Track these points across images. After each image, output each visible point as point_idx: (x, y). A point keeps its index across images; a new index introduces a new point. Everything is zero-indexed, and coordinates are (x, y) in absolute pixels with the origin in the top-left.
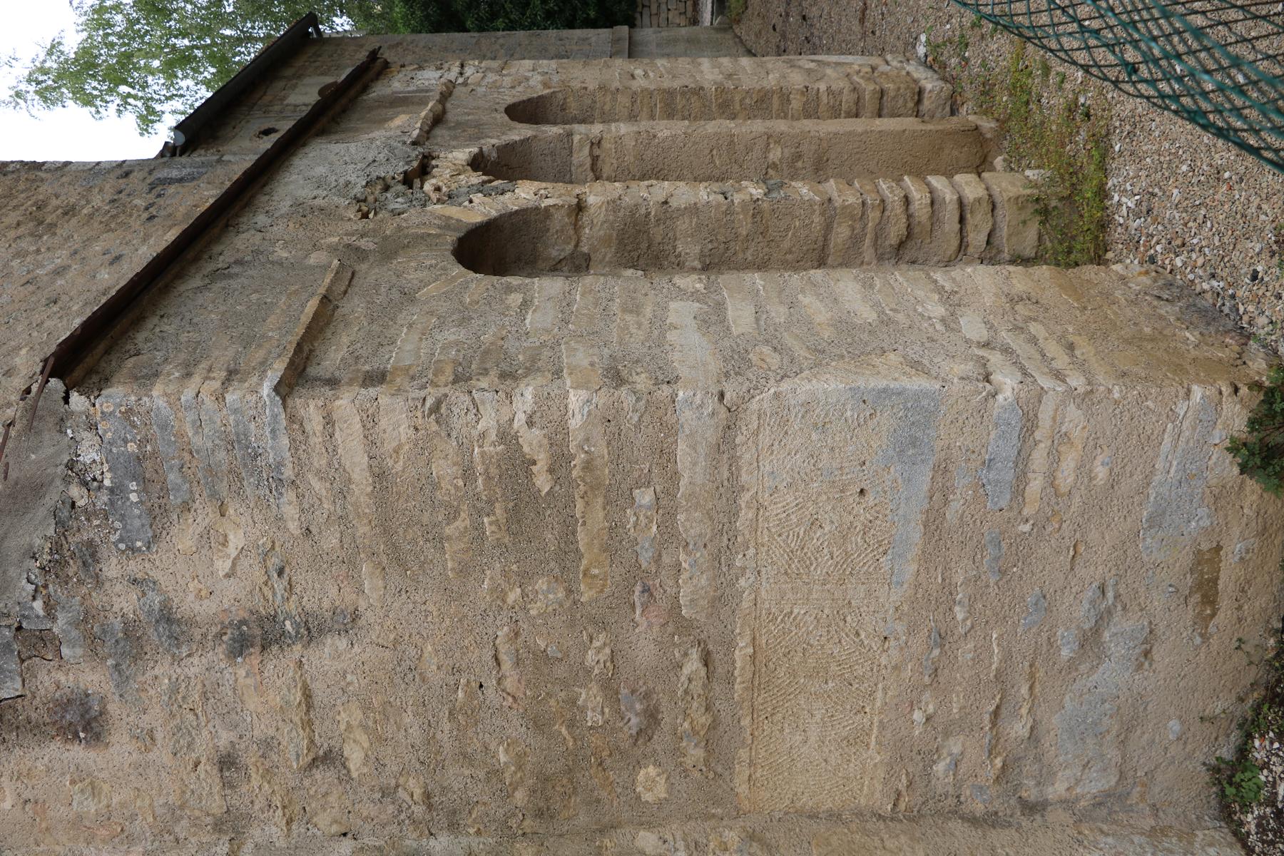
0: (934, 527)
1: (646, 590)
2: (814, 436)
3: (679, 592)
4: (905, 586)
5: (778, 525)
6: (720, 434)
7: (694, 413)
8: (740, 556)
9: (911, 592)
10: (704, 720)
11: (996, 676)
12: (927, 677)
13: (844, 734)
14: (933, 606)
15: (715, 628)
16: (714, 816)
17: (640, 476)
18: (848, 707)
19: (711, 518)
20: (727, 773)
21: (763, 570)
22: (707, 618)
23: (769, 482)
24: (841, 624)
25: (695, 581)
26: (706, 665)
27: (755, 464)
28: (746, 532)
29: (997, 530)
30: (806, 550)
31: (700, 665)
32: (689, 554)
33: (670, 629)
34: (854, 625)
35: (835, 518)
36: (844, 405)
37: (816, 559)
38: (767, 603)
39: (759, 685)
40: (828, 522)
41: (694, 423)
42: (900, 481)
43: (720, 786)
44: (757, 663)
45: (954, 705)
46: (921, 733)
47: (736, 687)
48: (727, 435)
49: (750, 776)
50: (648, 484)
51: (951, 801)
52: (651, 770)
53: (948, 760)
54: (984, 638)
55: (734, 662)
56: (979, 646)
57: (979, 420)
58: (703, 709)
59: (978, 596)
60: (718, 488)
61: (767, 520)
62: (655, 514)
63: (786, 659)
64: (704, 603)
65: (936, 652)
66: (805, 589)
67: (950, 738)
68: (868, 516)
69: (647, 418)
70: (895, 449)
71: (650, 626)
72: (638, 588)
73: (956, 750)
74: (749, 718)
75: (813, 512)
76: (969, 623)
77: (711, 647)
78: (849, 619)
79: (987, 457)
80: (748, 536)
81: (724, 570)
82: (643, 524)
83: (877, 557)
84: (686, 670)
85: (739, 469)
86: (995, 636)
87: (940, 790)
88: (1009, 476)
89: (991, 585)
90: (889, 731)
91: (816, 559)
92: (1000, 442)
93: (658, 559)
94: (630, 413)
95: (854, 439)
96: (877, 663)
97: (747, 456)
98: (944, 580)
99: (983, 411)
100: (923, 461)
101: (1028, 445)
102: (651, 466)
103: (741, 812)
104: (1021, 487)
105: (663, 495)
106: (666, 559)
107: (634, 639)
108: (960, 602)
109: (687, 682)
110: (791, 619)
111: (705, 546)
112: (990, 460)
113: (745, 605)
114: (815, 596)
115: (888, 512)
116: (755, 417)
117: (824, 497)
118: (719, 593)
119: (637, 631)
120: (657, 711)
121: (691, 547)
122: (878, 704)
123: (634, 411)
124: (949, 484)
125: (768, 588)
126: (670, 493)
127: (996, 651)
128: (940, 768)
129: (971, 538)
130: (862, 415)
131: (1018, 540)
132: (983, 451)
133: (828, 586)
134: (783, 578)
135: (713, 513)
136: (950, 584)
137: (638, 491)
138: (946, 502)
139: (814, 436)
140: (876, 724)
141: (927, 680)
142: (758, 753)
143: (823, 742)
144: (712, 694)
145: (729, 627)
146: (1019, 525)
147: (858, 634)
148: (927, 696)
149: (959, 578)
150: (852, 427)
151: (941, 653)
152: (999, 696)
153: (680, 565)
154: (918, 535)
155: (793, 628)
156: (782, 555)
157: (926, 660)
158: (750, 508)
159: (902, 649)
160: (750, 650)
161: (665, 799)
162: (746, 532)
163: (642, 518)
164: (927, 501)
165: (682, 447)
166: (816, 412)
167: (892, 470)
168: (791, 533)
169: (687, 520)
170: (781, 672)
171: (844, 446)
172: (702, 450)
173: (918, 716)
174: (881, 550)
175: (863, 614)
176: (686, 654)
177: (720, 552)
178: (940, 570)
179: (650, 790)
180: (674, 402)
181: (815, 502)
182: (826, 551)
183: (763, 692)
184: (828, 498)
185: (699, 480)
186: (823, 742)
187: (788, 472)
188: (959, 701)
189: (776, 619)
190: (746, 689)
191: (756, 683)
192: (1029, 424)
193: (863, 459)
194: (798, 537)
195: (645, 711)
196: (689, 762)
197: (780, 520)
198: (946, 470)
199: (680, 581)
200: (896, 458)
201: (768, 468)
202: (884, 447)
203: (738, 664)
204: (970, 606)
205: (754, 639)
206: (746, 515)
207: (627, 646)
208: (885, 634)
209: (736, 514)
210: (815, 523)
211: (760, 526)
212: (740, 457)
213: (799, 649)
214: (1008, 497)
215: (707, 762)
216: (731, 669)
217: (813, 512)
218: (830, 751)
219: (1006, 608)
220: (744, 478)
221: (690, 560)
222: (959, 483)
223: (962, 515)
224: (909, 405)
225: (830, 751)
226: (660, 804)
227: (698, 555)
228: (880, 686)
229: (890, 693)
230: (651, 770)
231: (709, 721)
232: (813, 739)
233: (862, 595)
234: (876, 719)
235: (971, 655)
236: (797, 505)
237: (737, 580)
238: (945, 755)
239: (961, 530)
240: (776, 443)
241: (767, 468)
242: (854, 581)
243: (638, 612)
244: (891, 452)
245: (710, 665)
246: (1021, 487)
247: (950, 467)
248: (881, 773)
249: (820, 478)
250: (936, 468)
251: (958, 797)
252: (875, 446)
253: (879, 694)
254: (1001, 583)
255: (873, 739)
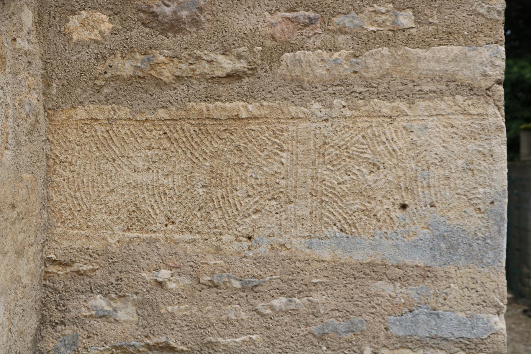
0: (368, 271)
1: (311, 21)
2: (460, 162)
3: (309, 50)
4: (308, 251)
5: (374, 135)
6: (466, 82)
7: (487, 59)
8: (344, 103)
9: (302, 256)
10: (167, 74)
11: (210, 342)
12: (209, 278)
13: (143, 207)
14: (285, 277)
15: (270, 83)
16: (49, 86)
17: (426, 15)
18: (175, 209)
19: (382, 77)
20: (102, 98)
21: (329, 124)
22: (280, 75)
23: (416, 125)
24: (269, 196)
25: (320, 64)
26: (228, 76)
27: (435, 113)
28: (367, 108)
29: (365, 328)
30: (348, 160)
31: (229, 70)
32: (347, 59)
33: (269, 43)
34: (267, 208)
35: (380, 184)
36: (490, 186)
37: (339, 170)
38: (294, 128)
39: (205, 125)
40: (375, 178)
41: (477, 59)
42: (415, 238)
43: (85, 91)
44: (229, 122)
45: (176, 307)
46: (143, 278)
47: (203, 103)
48: (464, 88)
49: (96, 120)
50: (418, 22)
51: (57, 316)
52: (107, 26)
53: (107, 308)
54: (251, 328)
55: (231, 101)
56: (243, 323)
57: (476, 302)
58: (178, 73)
59: (297, 317)
60: (413, 82)
61: (379, 125)
62: (388, 28)
63: (232, 148)
64: (297, 72)
65: (237, 284)
66: (308, 161)
67: (134, 308)
68: (381, 213)
69: (481, 20)
70: (446, 231)
71: (272, 25)
72: (312, 14)
73: (121, 315)
74: (167, 116)
75: (386, 165)
76: (268, 311)
77: (246, 80)
78: (274, 203)
79: (440, 311)
80: (363, 109)
81: (330, 89)
82: (377, 18)
83: (338, 224)
84: (221, 58)
85: (431, 99)
86: (254, 337)
87: (70, 304)
88: (422, 332)
89: (309, 328)
90: (146, 249)
91: (339, 170)
92: (455, 322)
93: (342, 31)
94: (486, 6)
95: (456, 196)
96: (223, 231)
97: (443, 105)
98: (315, 284)
99: (484, 304)
100: (434, 257)
101: (452, 347)
102: (435, 24)
103: (51, 112)
104: (410, 345)
105: (407, 35)
106: (341, 39)
107: (258, 10)
108: (291, 301)
109: (209, 59)
110: (275, 151)
111: (355, 72)
112: (438, 315)
113: (293, 109)
114: (300, 170)
115: (384, 230)
116: (481, 111)
117: (401, 173)
118: (306, 85)
119: (267, 13)
120: (175, 33)
121: (355, 60)
122: (177, 236)
123: (489, 10)
124: (411, 281)
125: (309, 129)
126: (409, 41)
127: (237, 340)
128: (99, 301)
129: (357, 305)
130: (479, 201)
131: (355, 348)
132: (446, 308)
133: (310, 182)
134: (320, 142)
135: (388, 79)
136: (310, 291)
137: (411, 13)
138: (392, 280)
139: (460, 162)
140: (154, 236)
141: (205, 279)
142: (123, 126)
143: (135, 187)
144: (195, 82)
145: (270, 95)
146: (371, 347)
147: (256, 211)
148: (187, 281)
149: (316, 298)
150: (468, 194)
151: (236, 289)
152: (185, 348)
153: (336, 51)
154: (360, 258)
155: (266, 153)
156: (343, 140)
157: (228, 276)
158: (392, 110)
159: (239, 253)
160: (244, 115)
161: (71, 39)
162: (367, 108)
163: (384, 17)
164: (395, 263)
165: (456, 50)
166: (482, 162)
167: (426, 231)
168: (366, 146)
169: (383, 56)
170: (218, 144)
171: (450, 187)
172: (451, 67)
173: (164, 274)
174: (346, 226)
175: (278, 216)
176: (240, 57)
177: (348, 86)
178: (325, 280)
179: (83, 25)
180: (496, 43)
181: (396, 166)
182: (347, 177)
183: (196, 129)
184: (400, 177)
185: (422, 65)
186: (135, 187)
187: (427, 141)
188: (180, 311)
189: (275, 138)
190: (201, 113)
191: (207, 122)
192: (473, 346)
193: (437, 204)
194: (362, 153)
195: (179, 20)
196: (117, 61)
197: (379, 136)
198: (424, 277)
199: (320, 51)
200: (437, 233)
201: (430, 124)
202: (448, 222)
203: (228, 105)
204: (286, 312)
205: (256, 118)
206: (386, 107)
207: (250, 4)
208: (256, 237)
209: (386, 98)
210: (375, 166)
211: (374, 120)
212: (442, 99)
213: (243, 159)
214: (401, 334)
215: (116, 78)
216: (222, 98)
217: (386, 165)
218: (123, 195)
219: (284, 345)
220: (422, 104)
221: (341, 59)
222: (413, 289)
223: (379, 295)
224: (489, 241)
225: (123, 195)
226: (66, 36)
227: (346, 66)
228: (197, 236)
229: (188, 246)
230: (107, 26)
231: (166, 80)
232: (138, 177)
233: (298, 213)
234: (160, 235)
235: (233, 317)
236: (394, 150)
237: (319, 101)
238: (114, 305)
239: (365, 296)
240: (455, 130)
241: (430, 123)
242: (314, 204)
243: (288, 14)
244: (443, 228)
245: (226, 80)
246: (410, 345)
247: (428, 281)
248: (95, 245)
249: (419, 169)
250: (428, 268)
251: (62, 323)
252: (450, 214)
253: (188, 236)
254: (310, 337)
255: (136, 235)
